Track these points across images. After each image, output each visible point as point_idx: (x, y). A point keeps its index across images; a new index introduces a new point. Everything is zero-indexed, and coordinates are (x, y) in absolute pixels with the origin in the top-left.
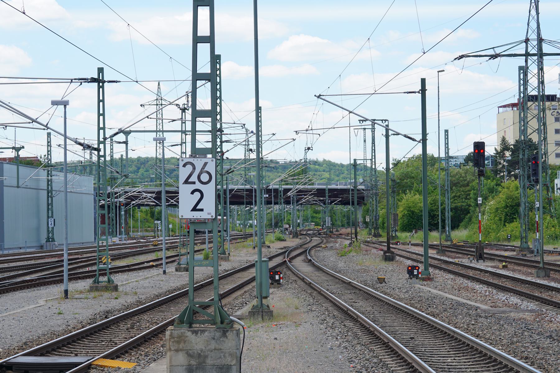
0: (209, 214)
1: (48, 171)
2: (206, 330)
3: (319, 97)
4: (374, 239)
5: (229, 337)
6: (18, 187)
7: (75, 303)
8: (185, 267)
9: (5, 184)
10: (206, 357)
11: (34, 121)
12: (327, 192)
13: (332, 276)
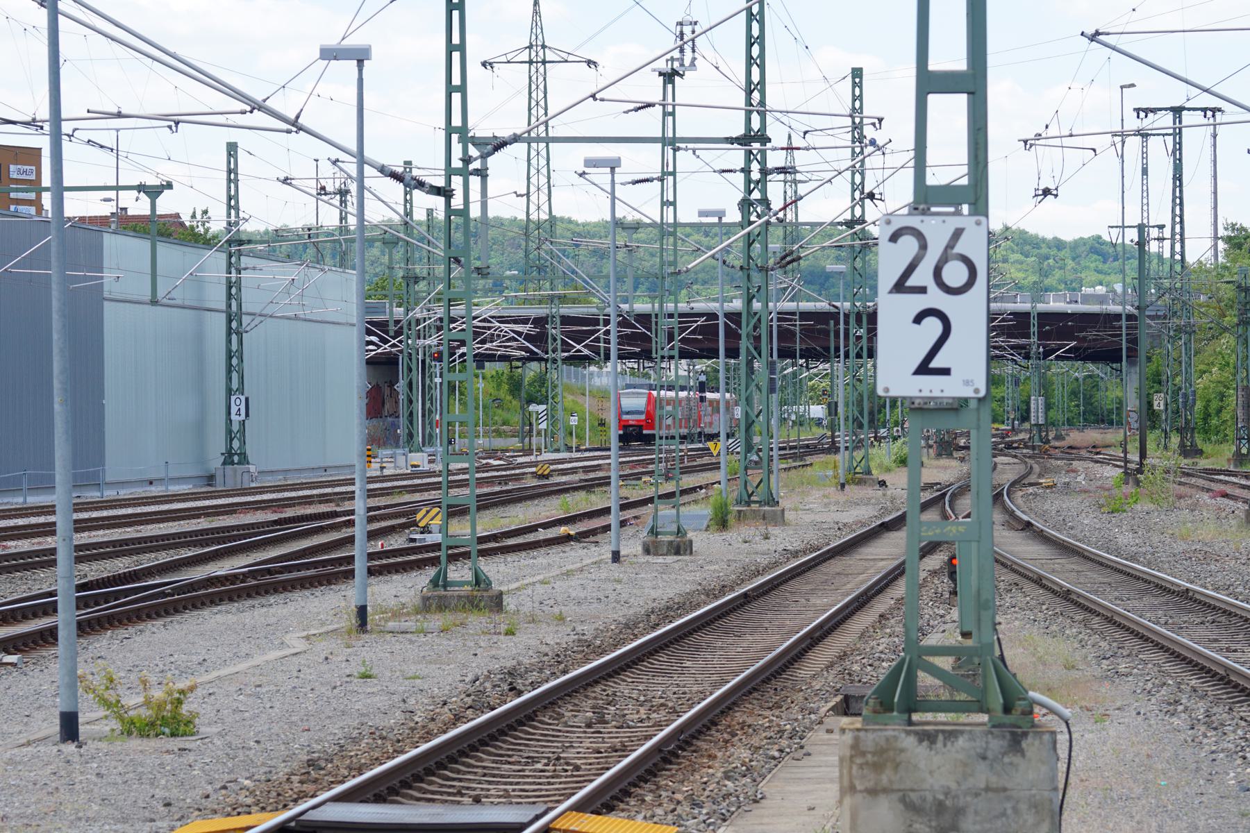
0: (967, 383)
1: (230, 256)
2: (962, 732)
3: (1094, 37)
4: (1185, 462)
5: (1028, 754)
6: (154, 302)
7: (396, 644)
8: (671, 543)
9: (106, 295)
10: (960, 812)
11: (257, 106)
12: (1034, 321)
13: (1120, 571)
